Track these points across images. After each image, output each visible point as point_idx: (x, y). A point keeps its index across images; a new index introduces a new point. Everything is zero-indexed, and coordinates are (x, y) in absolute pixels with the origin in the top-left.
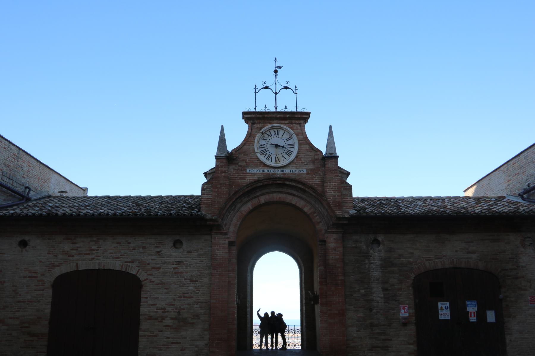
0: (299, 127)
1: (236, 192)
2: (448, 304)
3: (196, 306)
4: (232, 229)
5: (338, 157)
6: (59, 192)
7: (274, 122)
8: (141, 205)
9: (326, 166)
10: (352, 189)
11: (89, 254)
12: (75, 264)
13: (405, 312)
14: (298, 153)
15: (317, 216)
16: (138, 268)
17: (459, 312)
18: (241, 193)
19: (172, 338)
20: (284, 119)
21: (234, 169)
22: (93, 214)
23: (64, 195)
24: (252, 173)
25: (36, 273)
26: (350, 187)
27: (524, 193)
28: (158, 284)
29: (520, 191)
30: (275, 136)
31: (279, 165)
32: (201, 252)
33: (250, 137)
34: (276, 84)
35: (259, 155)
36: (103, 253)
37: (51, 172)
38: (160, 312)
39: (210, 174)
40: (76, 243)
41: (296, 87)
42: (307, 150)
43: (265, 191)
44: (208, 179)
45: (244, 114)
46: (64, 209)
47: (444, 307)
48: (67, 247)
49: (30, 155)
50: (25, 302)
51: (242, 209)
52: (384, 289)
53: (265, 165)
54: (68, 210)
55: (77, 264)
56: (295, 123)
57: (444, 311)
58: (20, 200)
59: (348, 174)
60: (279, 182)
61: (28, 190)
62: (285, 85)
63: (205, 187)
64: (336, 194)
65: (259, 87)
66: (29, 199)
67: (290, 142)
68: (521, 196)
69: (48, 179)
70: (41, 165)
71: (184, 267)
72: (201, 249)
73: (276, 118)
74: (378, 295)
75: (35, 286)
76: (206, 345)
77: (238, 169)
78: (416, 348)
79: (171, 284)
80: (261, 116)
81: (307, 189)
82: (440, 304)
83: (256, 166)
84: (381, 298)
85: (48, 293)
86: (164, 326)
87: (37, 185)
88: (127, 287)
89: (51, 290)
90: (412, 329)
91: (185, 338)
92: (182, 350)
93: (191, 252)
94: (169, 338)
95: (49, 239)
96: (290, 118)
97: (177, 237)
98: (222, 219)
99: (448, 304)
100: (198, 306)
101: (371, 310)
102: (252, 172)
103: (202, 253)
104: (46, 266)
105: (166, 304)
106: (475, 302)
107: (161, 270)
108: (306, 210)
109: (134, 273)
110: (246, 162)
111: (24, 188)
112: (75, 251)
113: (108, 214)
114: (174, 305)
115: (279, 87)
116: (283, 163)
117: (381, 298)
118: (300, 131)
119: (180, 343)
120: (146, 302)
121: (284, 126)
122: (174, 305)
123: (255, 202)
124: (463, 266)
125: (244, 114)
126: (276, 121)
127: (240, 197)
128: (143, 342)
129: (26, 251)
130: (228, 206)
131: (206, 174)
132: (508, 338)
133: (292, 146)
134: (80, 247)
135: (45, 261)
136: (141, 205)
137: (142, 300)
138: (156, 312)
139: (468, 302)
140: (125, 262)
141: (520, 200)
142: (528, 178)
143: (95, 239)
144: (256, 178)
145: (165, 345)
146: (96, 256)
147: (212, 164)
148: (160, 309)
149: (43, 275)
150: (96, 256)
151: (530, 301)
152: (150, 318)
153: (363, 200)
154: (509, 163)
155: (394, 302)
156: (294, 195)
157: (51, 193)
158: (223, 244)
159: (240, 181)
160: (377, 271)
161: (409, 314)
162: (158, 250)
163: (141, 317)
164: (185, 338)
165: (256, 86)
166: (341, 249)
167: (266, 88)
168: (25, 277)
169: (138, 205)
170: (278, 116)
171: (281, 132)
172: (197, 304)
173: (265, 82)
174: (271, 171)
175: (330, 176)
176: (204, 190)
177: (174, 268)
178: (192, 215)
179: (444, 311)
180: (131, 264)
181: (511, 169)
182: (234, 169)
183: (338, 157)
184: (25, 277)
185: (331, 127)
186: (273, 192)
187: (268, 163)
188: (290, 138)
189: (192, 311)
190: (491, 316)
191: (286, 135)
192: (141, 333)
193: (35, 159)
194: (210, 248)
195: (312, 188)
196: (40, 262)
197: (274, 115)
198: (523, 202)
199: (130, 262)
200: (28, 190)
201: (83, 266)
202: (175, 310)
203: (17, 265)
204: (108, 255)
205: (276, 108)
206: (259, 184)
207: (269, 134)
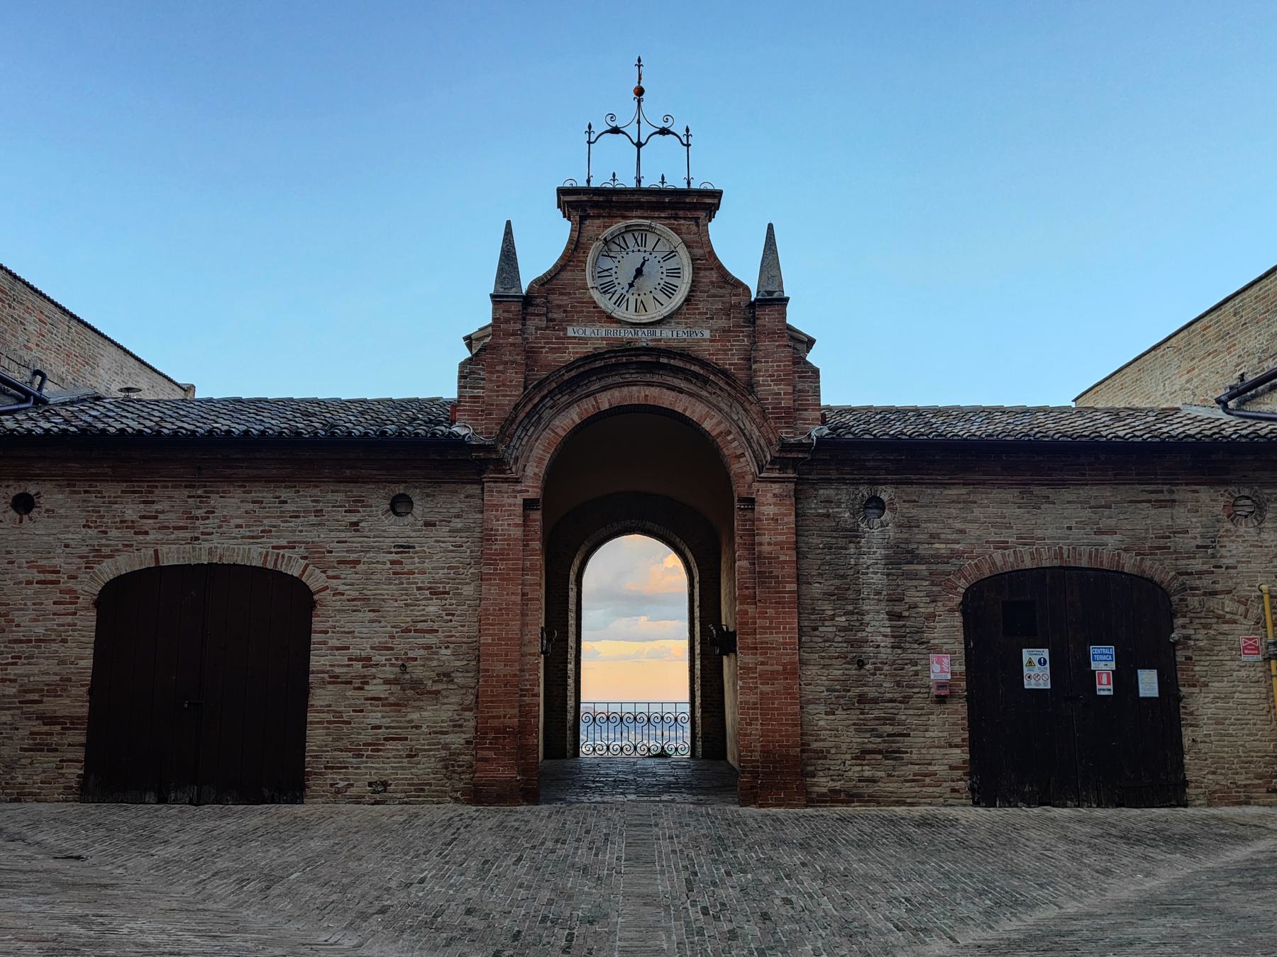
0: (694, 228)
1: (541, 384)
2: (1045, 653)
3: (443, 651)
4: (530, 471)
5: (787, 299)
6: (121, 390)
7: (634, 214)
8: (314, 415)
9: (758, 322)
10: (818, 377)
11: (186, 528)
12: (151, 552)
13: (942, 671)
14: (691, 291)
15: (734, 440)
16: (304, 562)
17: (1073, 672)
18: (554, 385)
19: (387, 728)
20: (659, 207)
21: (537, 329)
22: (194, 432)
23: (134, 396)
24: (580, 338)
25: (58, 572)
26: (816, 372)
27: (1231, 398)
28: (353, 600)
29: (1221, 393)
30: (636, 248)
31: (644, 318)
32: (458, 524)
33: (575, 249)
34: (639, 122)
35: (596, 295)
36: (220, 527)
37: (101, 340)
38: (358, 665)
39: (478, 339)
40: (153, 502)
41: (687, 130)
42: (712, 283)
43: (610, 381)
44: (474, 351)
45: (562, 192)
46: (124, 420)
47: (1035, 660)
48: (131, 510)
49: (45, 296)
50: (30, 641)
51: (557, 422)
52: (894, 616)
53: (610, 319)
54: (132, 423)
55: (156, 551)
56: (685, 218)
57: (1036, 670)
58: (21, 401)
59: (810, 342)
60: (645, 359)
61: (39, 378)
62: (662, 125)
63: (467, 373)
64: (782, 388)
65: (597, 130)
66: (41, 401)
67: (672, 264)
68: (1222, 403)
69: (94, 357)
70: (73, 322)
71: (417, 560)
72: (458, 516)
73: (640, 206)
74: (877, 628)
75: (55, 603)
76: (468, 742)
77: (547, 328)
78: (967, 757)
79: (383, 600)
80: (601, 199)
81: (712, 377)
82: (1026, 654)
83: (590, 320)
84: (886, 636)
85: (88, 620)
86: (367, 699)
87: (63, 369)
88: (281, 606)
89: (93, 614)
90: (959, 710)
91: (417, 727)
92: (409, 756)
93: (434, 525)
94: (379, 727)
95: (86, 492)
96: (673, 206)
97: (400, 489)
98: (508, 447)
99: (1045, 653)
100: (448, 652)
101: (861, 664)
102: (581, 334)
103: (459, 526)
104: (80, 557)
105: (372, 648)
106: (1111, 650)
107: (360, 567)
108: (707, 425)
109: (296, 574)
110: (565, 311)
111: (28, 373)
112: (151, 521)
113: (229, 432)
114: (392, 649)
115: (646, 130)
116: (655, 313)
117: (886, 636)
118: (696, 238)
119: (406, 739)
120: (325, 643)
121: (658, 225)
122: (392, 649)
123: (588, 407)
124: (1084, 563)
125: (562, 192)
126: (639, 213)
127: (551, 393)
128: (316, 738)
129: (30, 519)
130: (522, 415)
131: (469, 340)
132: (1187, 735)
133: (675, 273)
134: (163, 512)
135: (82, 543)
136: (314, 415)
137: (315, 637)
138: (348, 666)
139: (1094, 650)
140: (273, 548)
141: (1219, 413)
142: (1240, 360)
143: (200, 492)
144: (589, 348)
145: (369, 744)
146: (203, 533)
147: (482, 316)
148: (356, 660)
149: (75, 577)
150: (203, 533)
151: (1245, 648)
152: (335, 679)
153: (843, 411)
154: (1193, 327)
155: (916, 646)
156: (681, 391)
157: (102, 391)
158: (510, 505)
159: (551, 356)
160: (876, 573)
161: (953, 673)
162: (354, 519)
163: (311, 678)
164: (417, 727)
165: (590, 127)
166: (793, 518)
167: (615, 130)
168: (29, 583)
169: (306, 414)
170: (643, 199)
171: (651, 240)
172: (447, 648)
173: (613, 117)
174: (626, 334)
175: (766, 344)
176: (465, 377)
177: (392, 563)
178: (434, 434)
179: (1036, 670)
180: (287, 553)
181: (1197, 340)
182: (537, 329)
183: (787, 299)
184: (29, 583)
185: (770, 227)
186: (634, 384)
187: (619, 313)
188: (672, 254)
189: (435, 663)
190: (1148, 683)
191: (663, 248)
192: (311, 717)
193: (56, 305)
194: (479, 516)
195: (724, 373)
196: (67, 546)
197: (635, 198)
198: (1227, 418)
199: (284, 547)
200: (39, 378)
201: (172, 556)
202: (394, 661)
203: (9, 552)
204: (234, 530)
205: (639, 181)
206: (598, 364)
207: (622, 244)
